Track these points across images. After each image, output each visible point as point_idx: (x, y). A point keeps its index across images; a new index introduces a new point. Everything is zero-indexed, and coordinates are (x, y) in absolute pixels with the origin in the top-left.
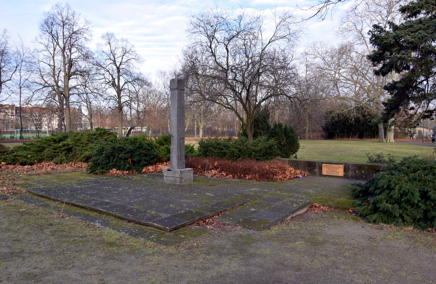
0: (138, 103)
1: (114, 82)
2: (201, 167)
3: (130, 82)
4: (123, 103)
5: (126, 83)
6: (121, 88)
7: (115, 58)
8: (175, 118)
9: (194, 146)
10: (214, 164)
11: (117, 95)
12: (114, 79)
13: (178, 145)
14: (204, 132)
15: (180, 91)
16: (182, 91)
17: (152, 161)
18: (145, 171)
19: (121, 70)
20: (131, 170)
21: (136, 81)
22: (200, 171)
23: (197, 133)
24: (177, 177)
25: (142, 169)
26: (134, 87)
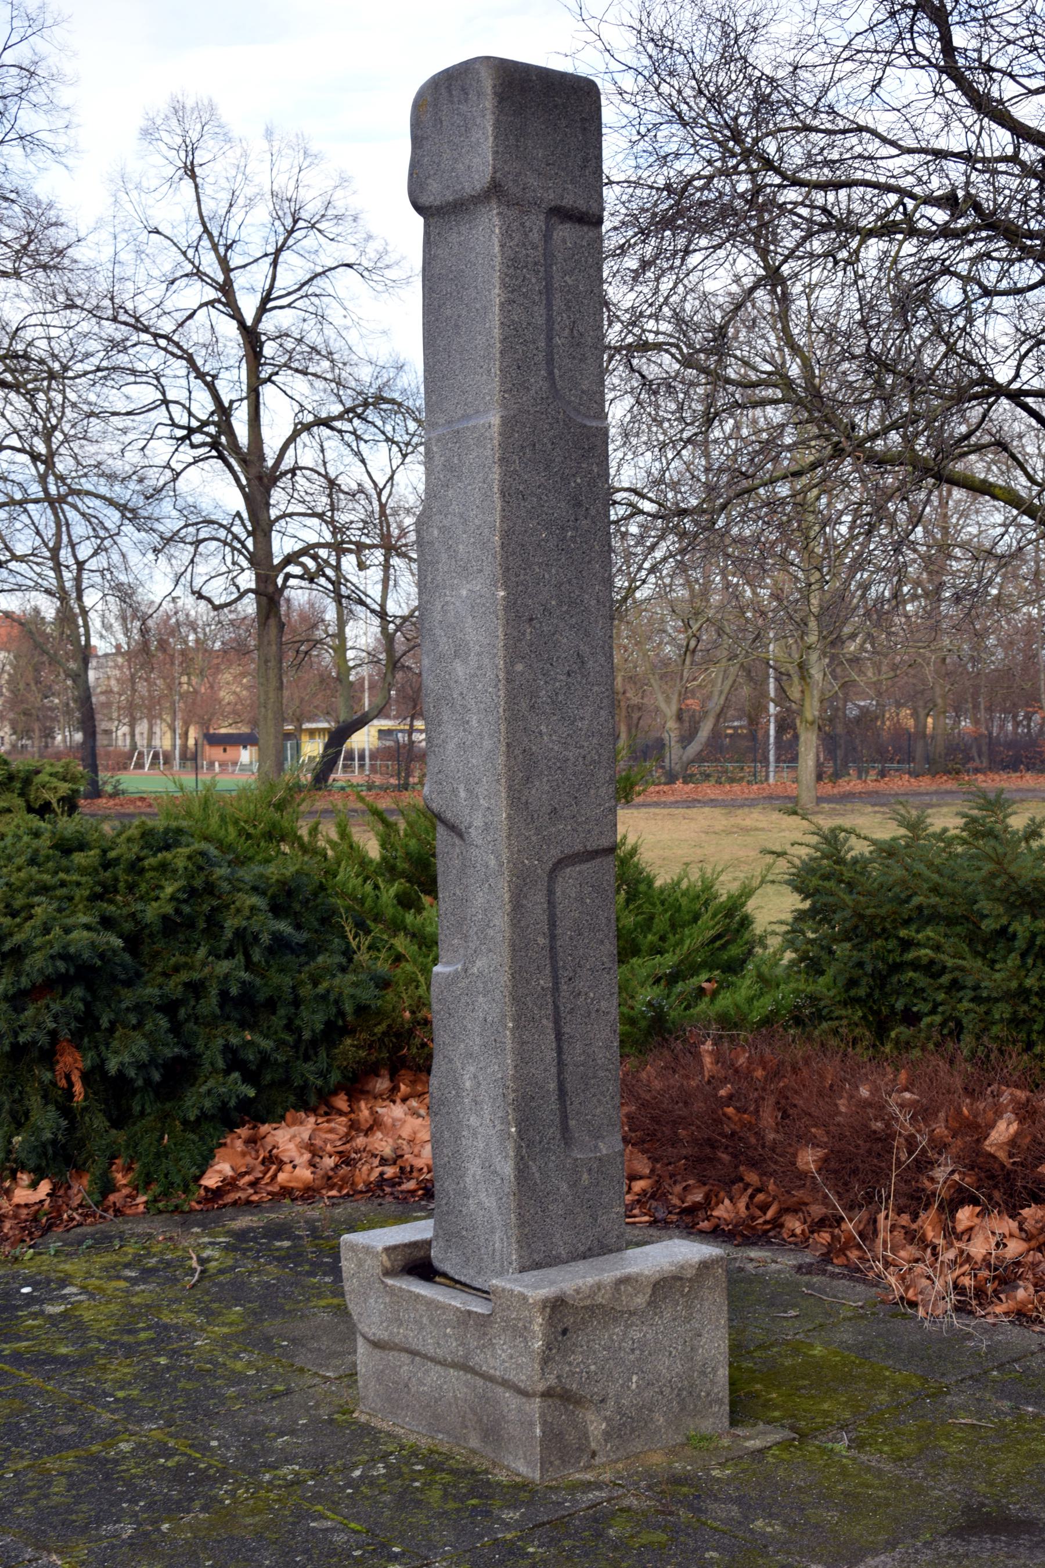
0: (386, 567)
1: (226, 427)
2: (824, 1163)
3: (326, 422)
4: (289, 560)
5: (301, 429)
6: (270, 463)
7: (227, 269)
8: (478, 585)
9: (747, 892)
10: (979, 1130)
11: (245, 515)
12: (223, 411)
13: (518, 948)
14: (829, 743)
15: (536, 222)
16: (565, 233)
17: (308, 1071)
18: (229, 1184)
19: (269, 349)
20: (80, 1170)
21: (371, 414)
22: (817, 1211)
23: (778, 760)
24: (505, 1383)
25: (205, 1163)
26: (363, 461)
